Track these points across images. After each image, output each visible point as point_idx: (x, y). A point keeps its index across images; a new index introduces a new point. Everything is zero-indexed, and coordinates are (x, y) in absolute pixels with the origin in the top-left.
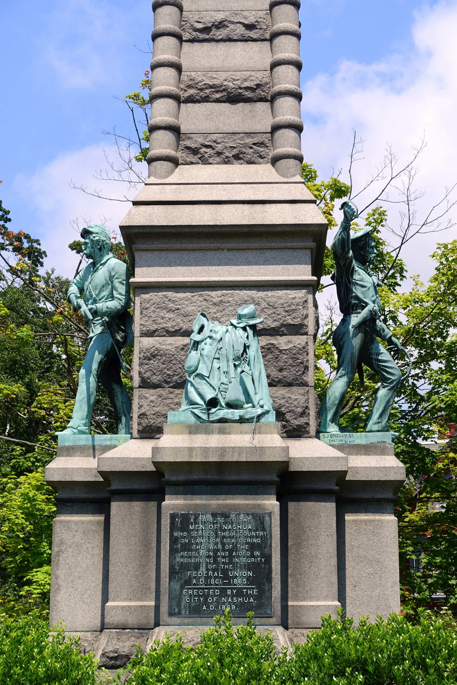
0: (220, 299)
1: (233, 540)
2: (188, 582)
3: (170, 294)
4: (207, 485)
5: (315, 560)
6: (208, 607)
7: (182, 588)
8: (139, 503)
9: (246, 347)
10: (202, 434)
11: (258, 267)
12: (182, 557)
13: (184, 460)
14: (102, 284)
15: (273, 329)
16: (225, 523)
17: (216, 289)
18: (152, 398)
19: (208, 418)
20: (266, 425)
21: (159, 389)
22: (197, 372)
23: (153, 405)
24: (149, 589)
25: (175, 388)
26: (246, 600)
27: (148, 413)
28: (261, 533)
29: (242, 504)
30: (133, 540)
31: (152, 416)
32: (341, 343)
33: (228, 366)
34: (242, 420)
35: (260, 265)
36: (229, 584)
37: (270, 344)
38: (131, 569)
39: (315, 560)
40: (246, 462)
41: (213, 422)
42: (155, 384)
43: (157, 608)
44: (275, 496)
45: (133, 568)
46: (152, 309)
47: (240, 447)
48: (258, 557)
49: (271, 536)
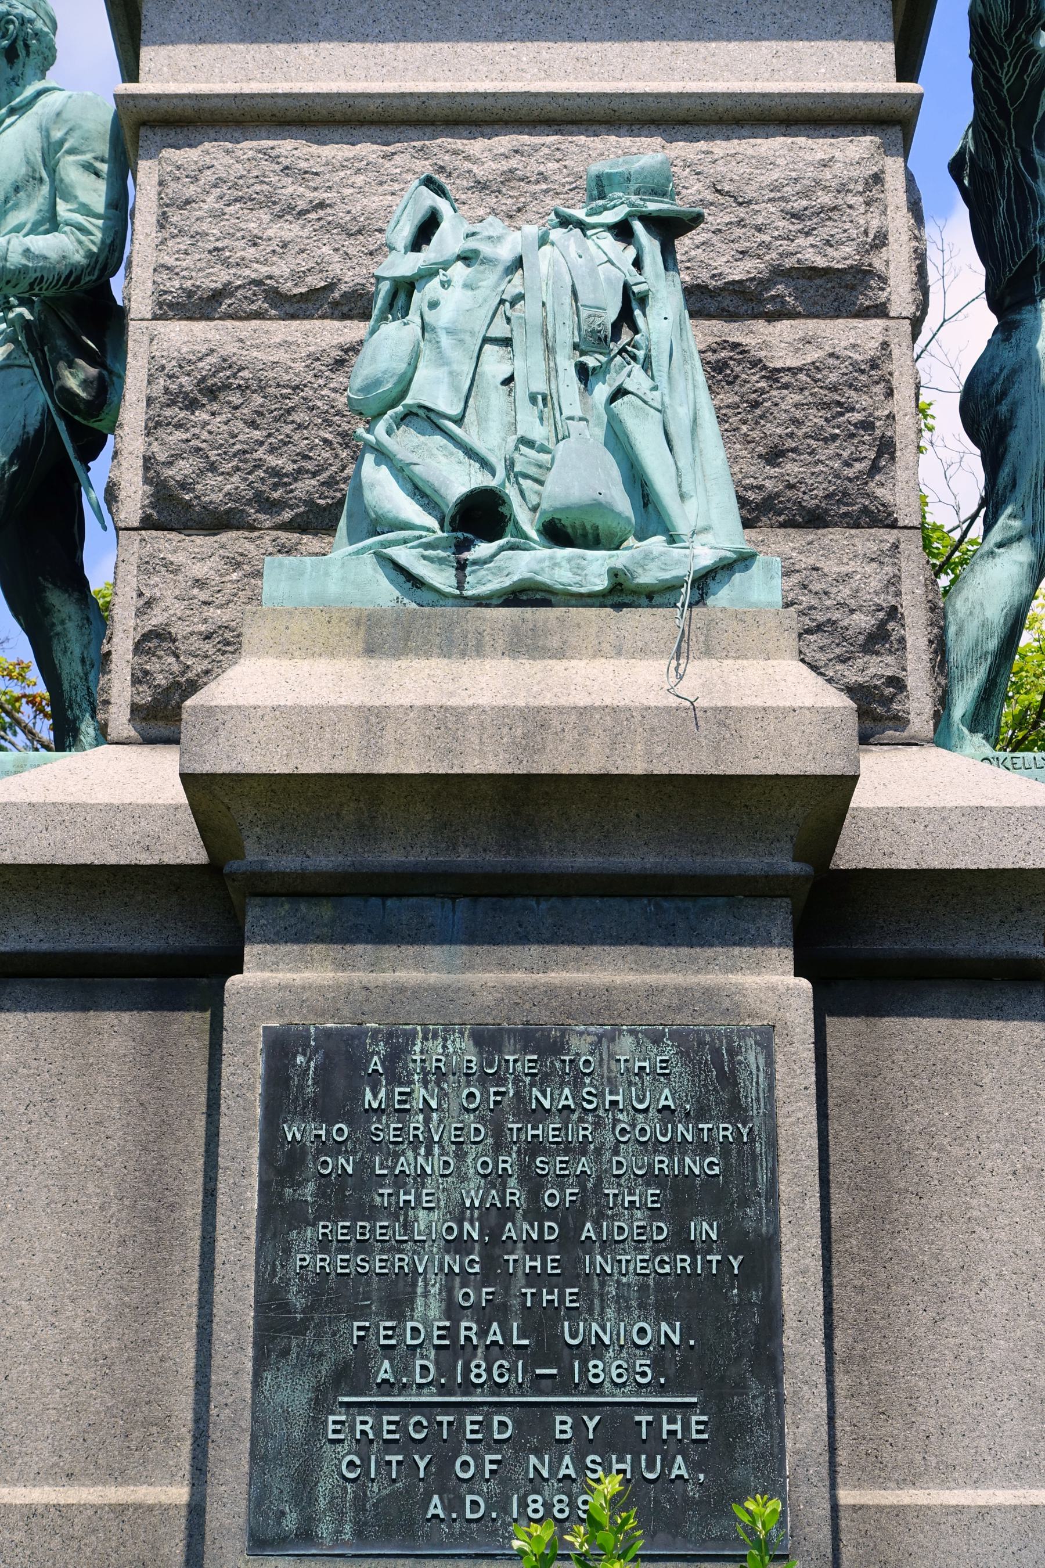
0: (505, 165)
1: (583, 1165)
2: (352, 1374)
3: (289, 148)
4: (453, 896)
5: (958, 1288)
6: (454, 1504)
7: (320, 1405)
8: (126, 1017)
9: (632, 302)
10: (428, 655)
11: (666, 48)
12: (324, 1245)
13: (340, 766)
14: (10, 178)
15: (737, 289)
16: (542, 1080)
17: (488, 130)
18: (199, 570)
19: (460, 586)
20: (737, 616)
21: (234, 534)
22: (408, 401)
23: (204, 596)
24: (164, 1423)
25: (303, 530)
26: (651, 1467)
27: (178, 630)
28: (725, 1130)
29: (626, 989)
30: (91, 1188)
31: (196, 644)
32: (1003, 409)
33: (551, 373)
34: (621, 593)
35: (674, 38)
36: (563, 1383)
37: (724, 345)
38: (77, 1326)
39: (958, 1288)
40: (649, 779)
41: (481, 602)
42: (214, 512)
43: (196, 1511)
44: (789, 953)
45: (89, 1322)
46: (211, 202)
47: (614, 709)
48: (708, 1246)
49: (773, 1145)
